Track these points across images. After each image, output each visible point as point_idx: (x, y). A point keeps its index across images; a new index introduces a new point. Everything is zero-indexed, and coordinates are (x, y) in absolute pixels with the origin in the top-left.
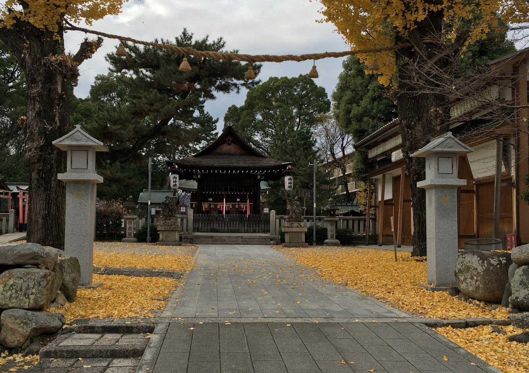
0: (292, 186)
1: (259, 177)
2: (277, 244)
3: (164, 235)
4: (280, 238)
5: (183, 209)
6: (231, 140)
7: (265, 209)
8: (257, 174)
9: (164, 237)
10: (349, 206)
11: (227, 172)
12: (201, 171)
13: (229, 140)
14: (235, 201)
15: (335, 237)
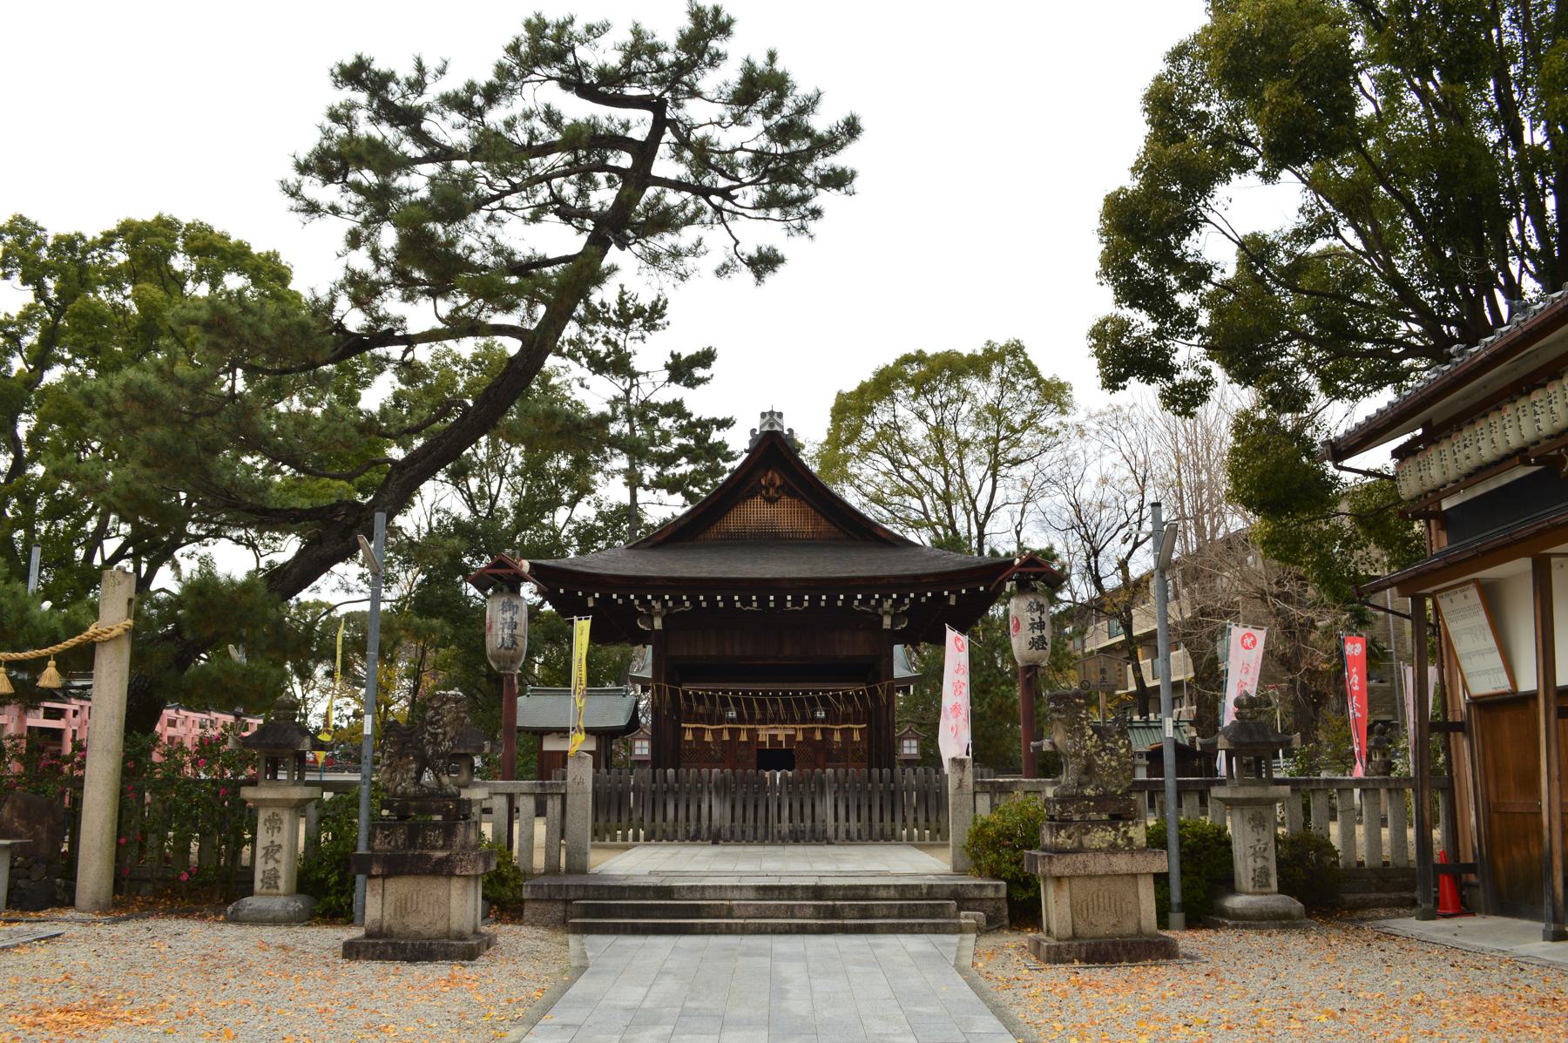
0: (1048, 640)
1: (887, 622)
2: (991, 926)
3: (389, 898)
4: (1003, 893)
6: (778, 483)
7: (906, 743)
8: (880, 611)
9: (389, 910)
11: (763, 601)
13: (772, 484)
15: (1274, 881)
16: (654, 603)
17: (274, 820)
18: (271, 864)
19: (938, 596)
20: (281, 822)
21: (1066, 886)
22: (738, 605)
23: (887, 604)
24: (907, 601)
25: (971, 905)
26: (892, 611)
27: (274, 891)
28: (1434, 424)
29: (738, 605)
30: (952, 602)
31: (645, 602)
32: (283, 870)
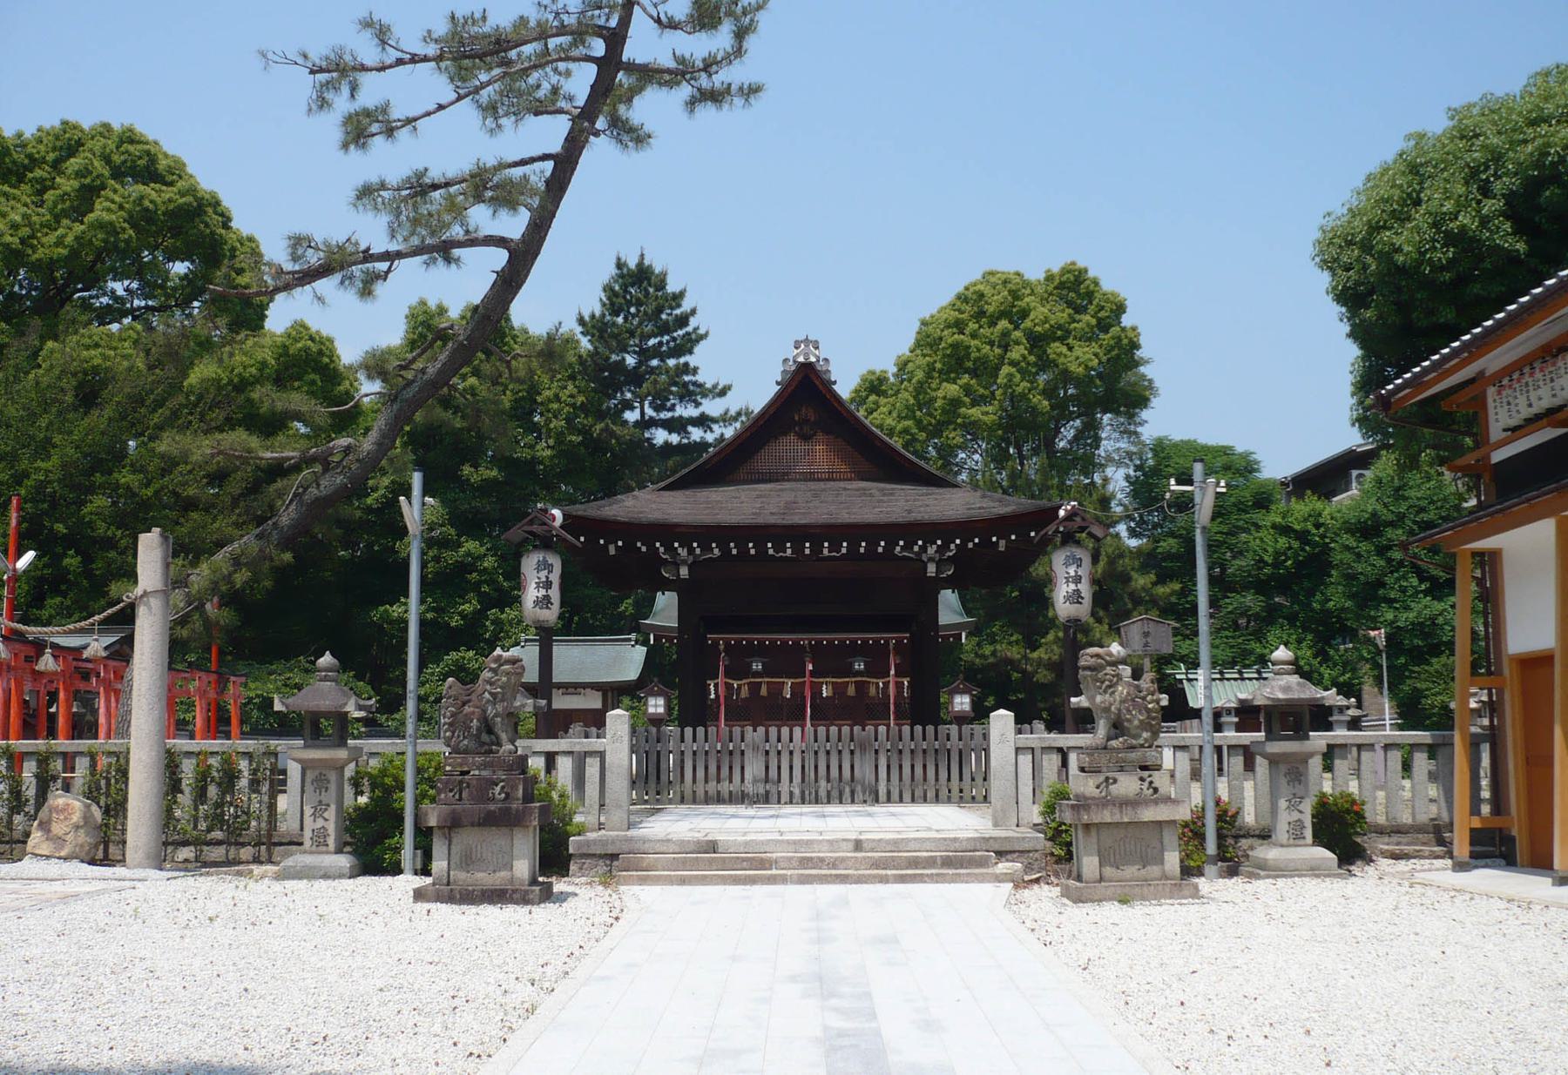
1: (931, 569)
5: (656, 706)
8: (924, 558)
10: (1250, 679)
12: (691, 551)
14: (850, 672)
16: (680, 550)
17: (321, 780)
18: (320, 823)
19: (986, 542)
20: (329, 782)
21: (1094, 832)
22: (771, 552)
23: (931, 550)
24: (952, 546)
25: (1009, 857)
26: (937, 557)
27: (324, 848)
28: (1487, 374)
29: (771, 552)
30: (1002, 549)
31: (670, 549)
32: (331, 828)
